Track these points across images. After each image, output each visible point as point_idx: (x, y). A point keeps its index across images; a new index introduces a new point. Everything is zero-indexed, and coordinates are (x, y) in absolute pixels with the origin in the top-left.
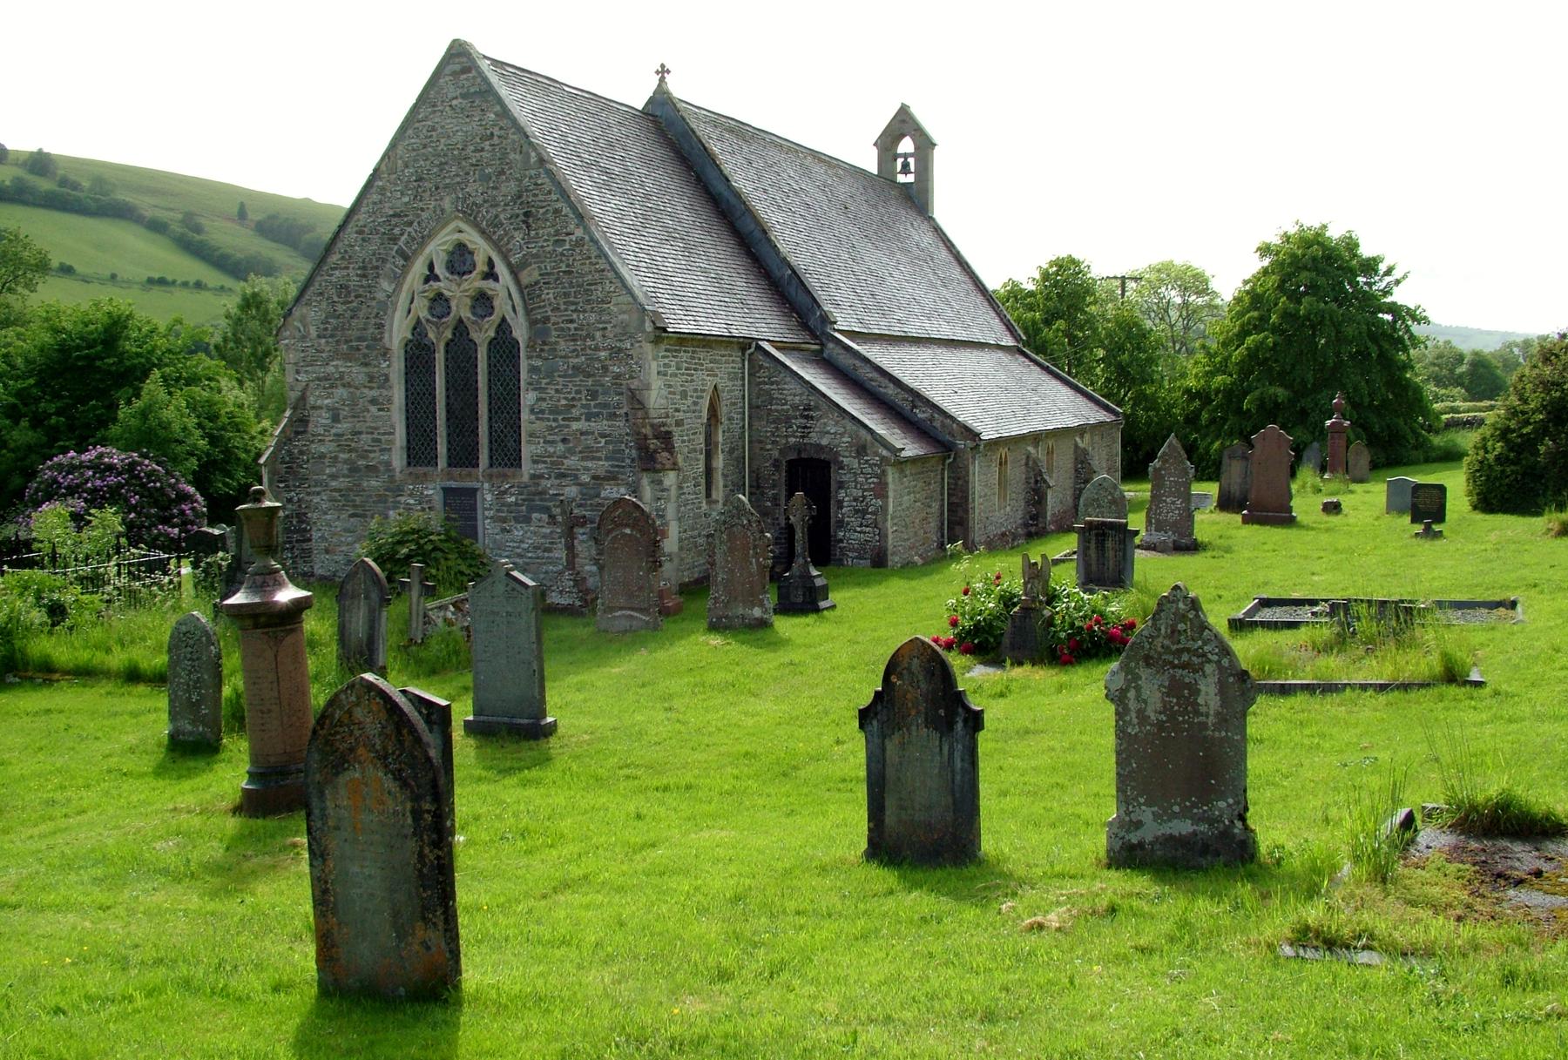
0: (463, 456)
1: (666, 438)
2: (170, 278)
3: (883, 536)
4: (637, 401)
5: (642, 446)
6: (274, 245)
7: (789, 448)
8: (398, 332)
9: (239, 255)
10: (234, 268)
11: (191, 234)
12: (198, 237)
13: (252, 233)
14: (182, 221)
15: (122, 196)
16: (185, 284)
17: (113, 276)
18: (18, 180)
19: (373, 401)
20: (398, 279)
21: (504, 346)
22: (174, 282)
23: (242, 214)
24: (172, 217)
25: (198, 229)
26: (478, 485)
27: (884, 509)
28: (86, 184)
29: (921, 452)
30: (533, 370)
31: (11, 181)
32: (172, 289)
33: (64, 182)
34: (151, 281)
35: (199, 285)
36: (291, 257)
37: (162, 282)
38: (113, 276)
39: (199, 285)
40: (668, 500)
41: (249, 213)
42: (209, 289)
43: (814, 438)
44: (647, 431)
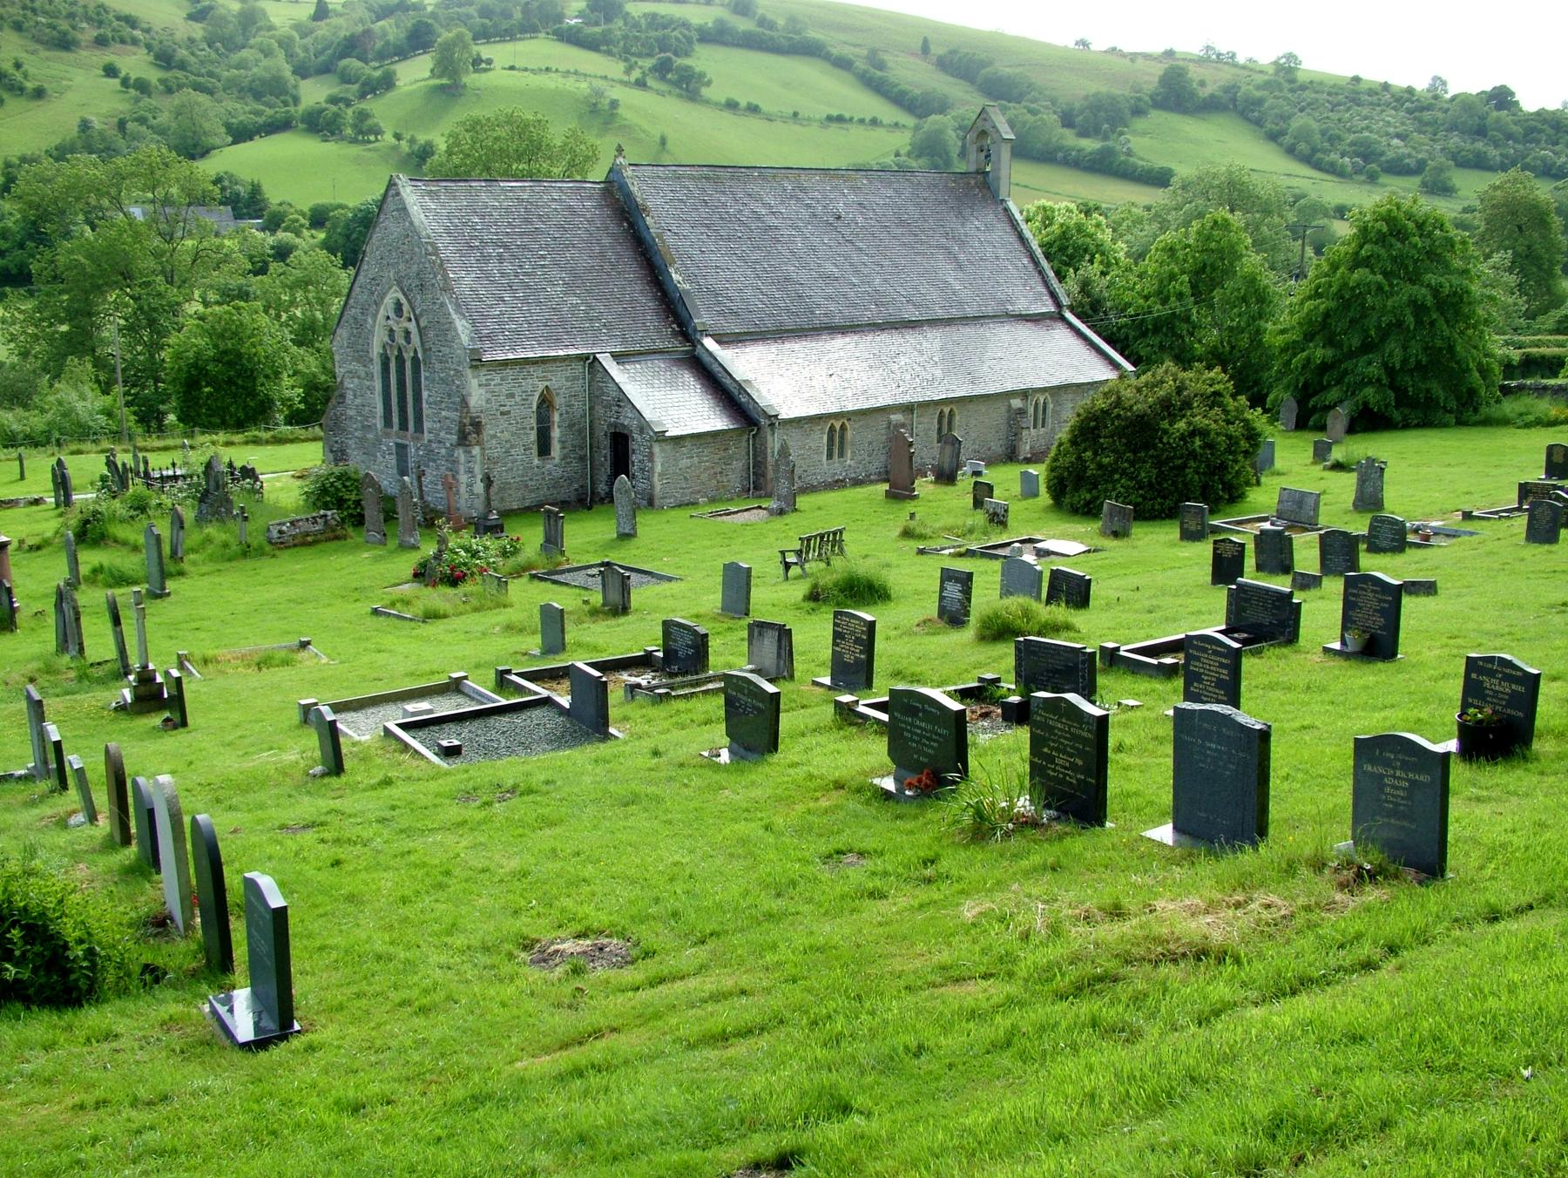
0: (404, 426)
1: (477, 426)
2: (847, 116)
3: (652, 486)
4: (464, 402)
5: (462, 426)
6: (952, 79)
7: (610, 425)
8: (376, 351)
9: (917, 92)
10: (916, 105)
11: (872, 70)
12: (879, 73)
13: (930, 67)
14: (867, 58)
15: (813, 34)
16: (862, 121)
17: (795, 114)
18: (720, 22)
19: (368, 388)
20: (375, 316)
21: (415, 360)
22: (851, 119)
23: (925, 49)
24: (857, 54)
25: (881, 66)
26: (407, 442)
27: (652, 468)
28: (781, 22)
29: (719, 427)
30: (426, 378)
31: (714, 22)
32: (848, 126)
33: (762, 22)
34: (830, 118)
35: (874, 122)
36: (967, 92)
37: (840, 119)
38: (795, 114)
39: (874, 122)
40: (475, 462)
41: (932, 47)
42: (884, 126)
43: (622, 420)
44: (467, 421)
